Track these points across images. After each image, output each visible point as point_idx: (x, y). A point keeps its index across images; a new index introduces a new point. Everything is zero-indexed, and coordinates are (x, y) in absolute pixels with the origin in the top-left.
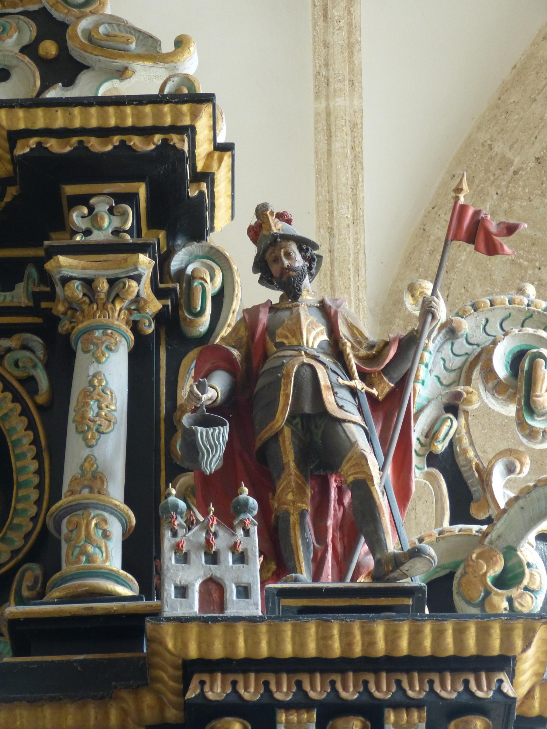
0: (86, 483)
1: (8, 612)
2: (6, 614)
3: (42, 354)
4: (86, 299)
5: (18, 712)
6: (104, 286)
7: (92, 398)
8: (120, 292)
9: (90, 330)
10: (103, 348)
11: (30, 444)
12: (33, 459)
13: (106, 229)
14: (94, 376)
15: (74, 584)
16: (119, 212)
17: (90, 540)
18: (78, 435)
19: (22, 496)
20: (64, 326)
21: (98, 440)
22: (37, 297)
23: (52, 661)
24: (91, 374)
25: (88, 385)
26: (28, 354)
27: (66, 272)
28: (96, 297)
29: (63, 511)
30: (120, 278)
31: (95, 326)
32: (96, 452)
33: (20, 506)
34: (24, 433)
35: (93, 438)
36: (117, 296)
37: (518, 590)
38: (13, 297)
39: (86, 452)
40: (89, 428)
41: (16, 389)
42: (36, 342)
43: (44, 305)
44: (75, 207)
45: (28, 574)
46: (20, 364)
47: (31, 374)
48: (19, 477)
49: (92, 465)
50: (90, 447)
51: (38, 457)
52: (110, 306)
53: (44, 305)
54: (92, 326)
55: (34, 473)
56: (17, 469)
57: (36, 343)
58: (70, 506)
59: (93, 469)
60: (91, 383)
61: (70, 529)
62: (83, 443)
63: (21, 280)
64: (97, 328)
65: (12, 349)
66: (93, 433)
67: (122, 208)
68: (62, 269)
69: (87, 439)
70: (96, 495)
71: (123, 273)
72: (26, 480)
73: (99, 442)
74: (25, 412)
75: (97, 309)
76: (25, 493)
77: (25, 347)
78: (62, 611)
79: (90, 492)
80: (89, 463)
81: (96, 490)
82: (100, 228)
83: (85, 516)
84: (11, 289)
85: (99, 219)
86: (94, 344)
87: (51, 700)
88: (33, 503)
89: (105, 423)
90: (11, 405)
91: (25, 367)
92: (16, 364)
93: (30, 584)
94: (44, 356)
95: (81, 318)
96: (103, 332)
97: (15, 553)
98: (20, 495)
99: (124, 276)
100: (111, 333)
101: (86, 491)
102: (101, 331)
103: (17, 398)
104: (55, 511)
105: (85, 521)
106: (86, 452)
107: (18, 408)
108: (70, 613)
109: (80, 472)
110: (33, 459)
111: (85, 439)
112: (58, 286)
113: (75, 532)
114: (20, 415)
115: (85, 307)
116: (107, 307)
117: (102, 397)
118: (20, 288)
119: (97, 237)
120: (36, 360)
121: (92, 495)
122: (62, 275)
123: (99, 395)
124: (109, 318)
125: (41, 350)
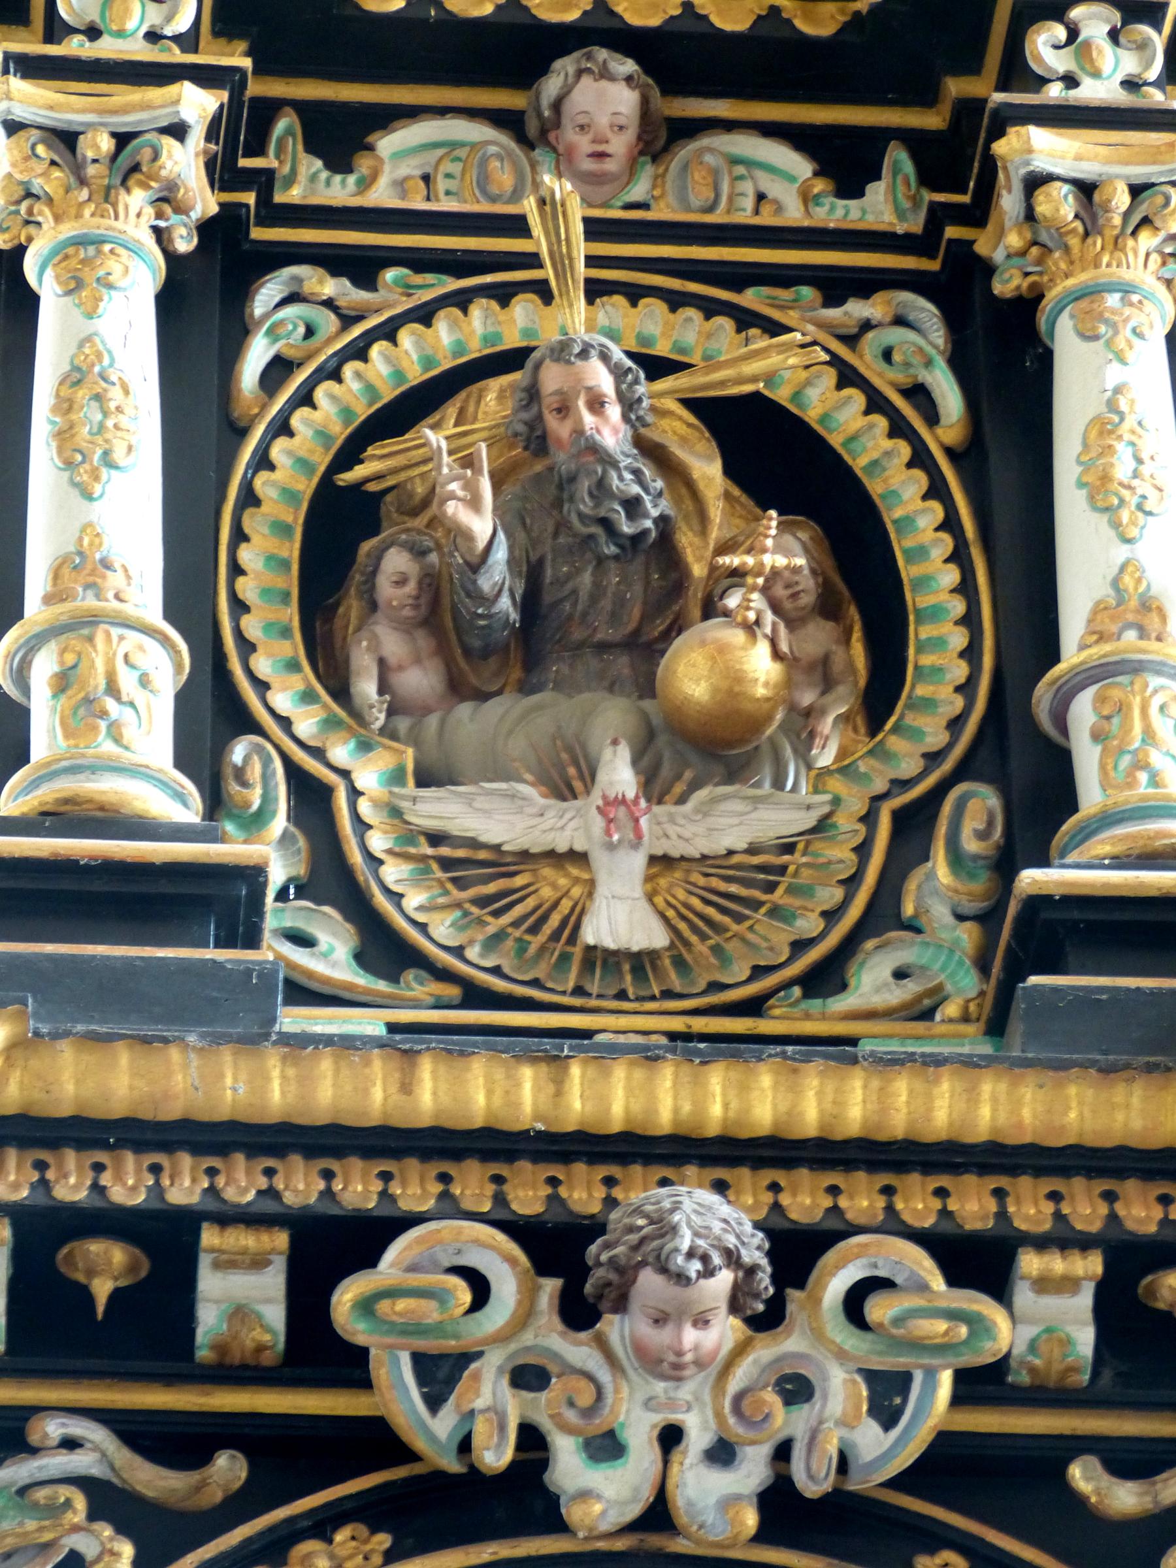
0: (1130, 617)
1: (1028, 881)
2: (1023, 884)
3: (939, 337)
4: (1078, 225)
5: (1072, 1090)
6: (1122, 199)
7: (1120, 437)
8: (1155, 214)
9: (1092, 292)
10: (1128, 332)
11: (937, 529)
12: (947, 561)
13: (1109, 77)
14: (1118, 390)
15: (1146, 830)
16: (1135, 42)
17: (1153, 738)
18: (1097, 515)
19: (929, 639)
20: (1007, 281)
21: (1143, 528)
22: (938, 217)
23: (1138, 989)
24: (1110, 385)
25: (1106, 410)
26: (911, 335)
27: (1042, 164)
28: (1101, 221)
29: (1084, 676)
30: (1153, 185)
31: (1104, 284)
32: (1143, 552)
33: (927, 660)
34: (920, 504)
35: (1133, 523)
36: (1146, 221)
37: (960, 918)
38: (864, 212)
39: (1122, 553)
40: (1122, 501)
41: (896, 410)
42: (924, 310)
43: (952, 232)
44: (1040, 24)
45: (973, 805)
46: (897, 357)
47: (920, 379)
48: (917, 599)
49: (1139, 581)
50: (1128, 541)
51: (959, 556)
52: (1130, 243)
53: (952, 232)
54: (1098, 285)
55: (952, 591)
56: (911, 580)
57: (923, 315)
58: (1101, 665)
59: (1140, 590)
60: (1112, 405)
61: (1105, 713)
62: (1112, 533)
63: (878, 178)
64: (1110, 288)
65: (874, 322)
66: (1132, 513)
67: (1140, 33)
68: (1033, 156)
69: (1120, 525)
70: (1154, 645)
71: (1161, 173)
72: (933, 606)
73: (1145, 531)
74: (920, 459)
75: (1103, 248)
76: (935, 633)
77: (900, 321)
78: (1142, 885)
79: (1141, 638)
80: (1132, 576)
81: (1154, 635)
82: (1096, 74)
83: (1137, 687)
84: (858, 193)
85: (1095, 54)
86: (1106, 322)
87: (1150, 1068)
88: (955, 655)
89: (1152, 494)
90: (888, 444)
91: (907, 365)
92: (887, 355)
93: (981, 826)
94: (946, 343)
95: (1063, 266)
96: (1122, 299)
97: (933, 758)
98: (923, 636)
99: (1163, 180)
100: (1140, 302)
101: (1131, 635)
102: (1117, 296)
103: (899, 428)
104: (1066, 674)
105: (1138, 699)
106: (1122, 553)
107: (904, 450)
108: (1160, 889)
109: (1112, 592)
110: (947, 561)
111: (1116, 525)
112: (1010, 191)
113: (1116, 721)
114: (910, 465)
115: (1074, 242)
116: (1125, 245)
117: (1140, 437)
118: (877, 192)
119: (1092, 92)
120: (933, 352)
121: (1143, 644)
122: (1032, 168)
123: (1133, 432)
124: (1128, 267)
125: (937, 331)
